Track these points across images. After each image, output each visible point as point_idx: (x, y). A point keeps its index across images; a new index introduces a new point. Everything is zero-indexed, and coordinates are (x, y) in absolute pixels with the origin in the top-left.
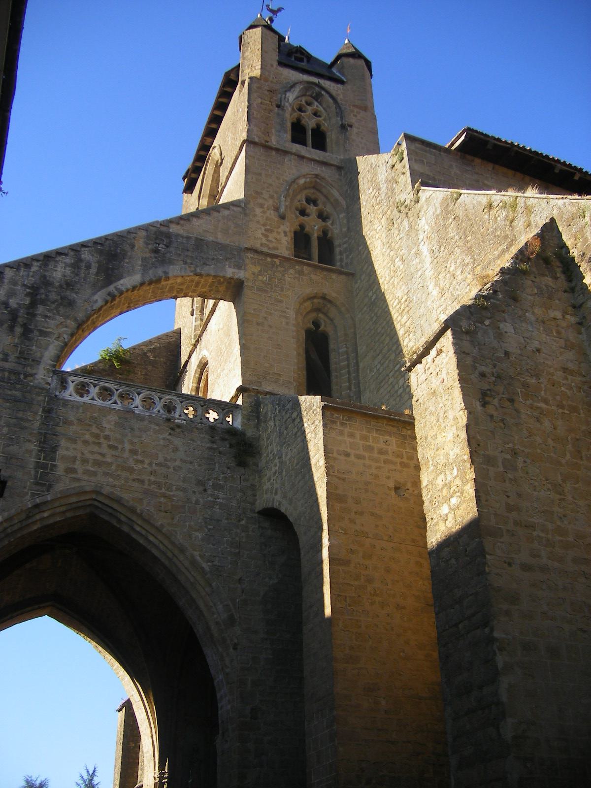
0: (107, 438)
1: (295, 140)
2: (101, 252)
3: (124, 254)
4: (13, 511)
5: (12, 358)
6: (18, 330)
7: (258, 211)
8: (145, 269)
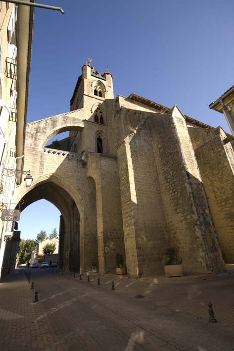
1: (95, 94)
2: (52, 121)
5: (33, 145)
6: (34, 139)
8: (62, 124)
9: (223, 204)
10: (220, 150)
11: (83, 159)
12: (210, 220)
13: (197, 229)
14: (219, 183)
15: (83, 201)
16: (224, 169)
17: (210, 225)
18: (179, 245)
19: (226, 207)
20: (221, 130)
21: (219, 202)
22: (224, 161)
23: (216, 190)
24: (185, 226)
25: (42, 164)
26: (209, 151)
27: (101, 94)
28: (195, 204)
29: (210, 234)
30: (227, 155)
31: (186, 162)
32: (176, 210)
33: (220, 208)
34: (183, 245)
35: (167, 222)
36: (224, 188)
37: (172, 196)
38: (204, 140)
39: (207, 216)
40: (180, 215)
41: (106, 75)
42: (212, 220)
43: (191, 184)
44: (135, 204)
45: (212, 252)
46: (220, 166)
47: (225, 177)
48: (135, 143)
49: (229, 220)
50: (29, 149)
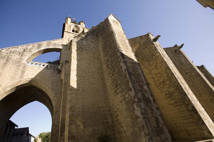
0: (35, 70)
3: (42, 45)
4: (14, 82)
6: (20, 55)
7: (65, 40)
9: (162, 86)
10: (151, 46)
11: (59, 68)
12: (150, 96)
13: (135, 107)
14: (155, 70)
15: (55, 98)
16: (157, 58)
17: (150, 102)
18: (121, 128)
19: (164, 88)
20: (150, 34)
21: (158, 85)
22: (156, 53)
23: (154, 76)
24: (125, 106)
25: (23, 72)
26: (144, 49)
27: (76, 32)
28: (131, 80)
29: (152, 112)
30: (158, 48)
31: (121, 46)
32: (116, 91)
33: (160, 90)
34: (125, 128)
35: (111, 105)
36: (159, 73)
37: (112, 79)
38: (140, 43)
39: (146, 92)
40: (120, 95)
41: (81, 23)
42: (152, 96)
43: (125, 62)
44: (74, 88)
45: (157, 136)
46: (154, 57)
47: (159, 64)
48: (82, 42)
49: (169, 99)
50: (15, 61)
